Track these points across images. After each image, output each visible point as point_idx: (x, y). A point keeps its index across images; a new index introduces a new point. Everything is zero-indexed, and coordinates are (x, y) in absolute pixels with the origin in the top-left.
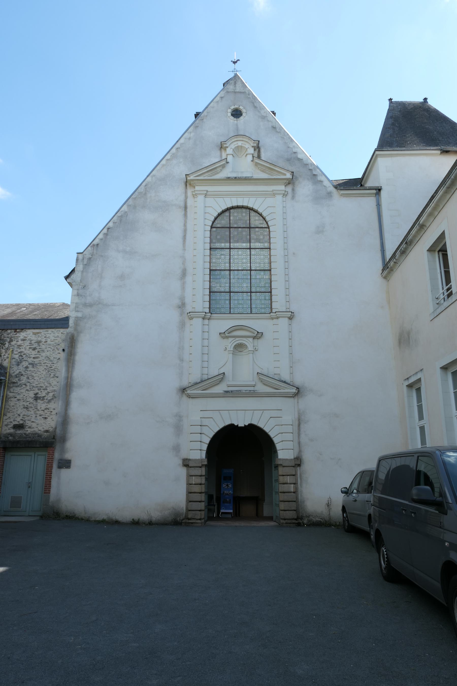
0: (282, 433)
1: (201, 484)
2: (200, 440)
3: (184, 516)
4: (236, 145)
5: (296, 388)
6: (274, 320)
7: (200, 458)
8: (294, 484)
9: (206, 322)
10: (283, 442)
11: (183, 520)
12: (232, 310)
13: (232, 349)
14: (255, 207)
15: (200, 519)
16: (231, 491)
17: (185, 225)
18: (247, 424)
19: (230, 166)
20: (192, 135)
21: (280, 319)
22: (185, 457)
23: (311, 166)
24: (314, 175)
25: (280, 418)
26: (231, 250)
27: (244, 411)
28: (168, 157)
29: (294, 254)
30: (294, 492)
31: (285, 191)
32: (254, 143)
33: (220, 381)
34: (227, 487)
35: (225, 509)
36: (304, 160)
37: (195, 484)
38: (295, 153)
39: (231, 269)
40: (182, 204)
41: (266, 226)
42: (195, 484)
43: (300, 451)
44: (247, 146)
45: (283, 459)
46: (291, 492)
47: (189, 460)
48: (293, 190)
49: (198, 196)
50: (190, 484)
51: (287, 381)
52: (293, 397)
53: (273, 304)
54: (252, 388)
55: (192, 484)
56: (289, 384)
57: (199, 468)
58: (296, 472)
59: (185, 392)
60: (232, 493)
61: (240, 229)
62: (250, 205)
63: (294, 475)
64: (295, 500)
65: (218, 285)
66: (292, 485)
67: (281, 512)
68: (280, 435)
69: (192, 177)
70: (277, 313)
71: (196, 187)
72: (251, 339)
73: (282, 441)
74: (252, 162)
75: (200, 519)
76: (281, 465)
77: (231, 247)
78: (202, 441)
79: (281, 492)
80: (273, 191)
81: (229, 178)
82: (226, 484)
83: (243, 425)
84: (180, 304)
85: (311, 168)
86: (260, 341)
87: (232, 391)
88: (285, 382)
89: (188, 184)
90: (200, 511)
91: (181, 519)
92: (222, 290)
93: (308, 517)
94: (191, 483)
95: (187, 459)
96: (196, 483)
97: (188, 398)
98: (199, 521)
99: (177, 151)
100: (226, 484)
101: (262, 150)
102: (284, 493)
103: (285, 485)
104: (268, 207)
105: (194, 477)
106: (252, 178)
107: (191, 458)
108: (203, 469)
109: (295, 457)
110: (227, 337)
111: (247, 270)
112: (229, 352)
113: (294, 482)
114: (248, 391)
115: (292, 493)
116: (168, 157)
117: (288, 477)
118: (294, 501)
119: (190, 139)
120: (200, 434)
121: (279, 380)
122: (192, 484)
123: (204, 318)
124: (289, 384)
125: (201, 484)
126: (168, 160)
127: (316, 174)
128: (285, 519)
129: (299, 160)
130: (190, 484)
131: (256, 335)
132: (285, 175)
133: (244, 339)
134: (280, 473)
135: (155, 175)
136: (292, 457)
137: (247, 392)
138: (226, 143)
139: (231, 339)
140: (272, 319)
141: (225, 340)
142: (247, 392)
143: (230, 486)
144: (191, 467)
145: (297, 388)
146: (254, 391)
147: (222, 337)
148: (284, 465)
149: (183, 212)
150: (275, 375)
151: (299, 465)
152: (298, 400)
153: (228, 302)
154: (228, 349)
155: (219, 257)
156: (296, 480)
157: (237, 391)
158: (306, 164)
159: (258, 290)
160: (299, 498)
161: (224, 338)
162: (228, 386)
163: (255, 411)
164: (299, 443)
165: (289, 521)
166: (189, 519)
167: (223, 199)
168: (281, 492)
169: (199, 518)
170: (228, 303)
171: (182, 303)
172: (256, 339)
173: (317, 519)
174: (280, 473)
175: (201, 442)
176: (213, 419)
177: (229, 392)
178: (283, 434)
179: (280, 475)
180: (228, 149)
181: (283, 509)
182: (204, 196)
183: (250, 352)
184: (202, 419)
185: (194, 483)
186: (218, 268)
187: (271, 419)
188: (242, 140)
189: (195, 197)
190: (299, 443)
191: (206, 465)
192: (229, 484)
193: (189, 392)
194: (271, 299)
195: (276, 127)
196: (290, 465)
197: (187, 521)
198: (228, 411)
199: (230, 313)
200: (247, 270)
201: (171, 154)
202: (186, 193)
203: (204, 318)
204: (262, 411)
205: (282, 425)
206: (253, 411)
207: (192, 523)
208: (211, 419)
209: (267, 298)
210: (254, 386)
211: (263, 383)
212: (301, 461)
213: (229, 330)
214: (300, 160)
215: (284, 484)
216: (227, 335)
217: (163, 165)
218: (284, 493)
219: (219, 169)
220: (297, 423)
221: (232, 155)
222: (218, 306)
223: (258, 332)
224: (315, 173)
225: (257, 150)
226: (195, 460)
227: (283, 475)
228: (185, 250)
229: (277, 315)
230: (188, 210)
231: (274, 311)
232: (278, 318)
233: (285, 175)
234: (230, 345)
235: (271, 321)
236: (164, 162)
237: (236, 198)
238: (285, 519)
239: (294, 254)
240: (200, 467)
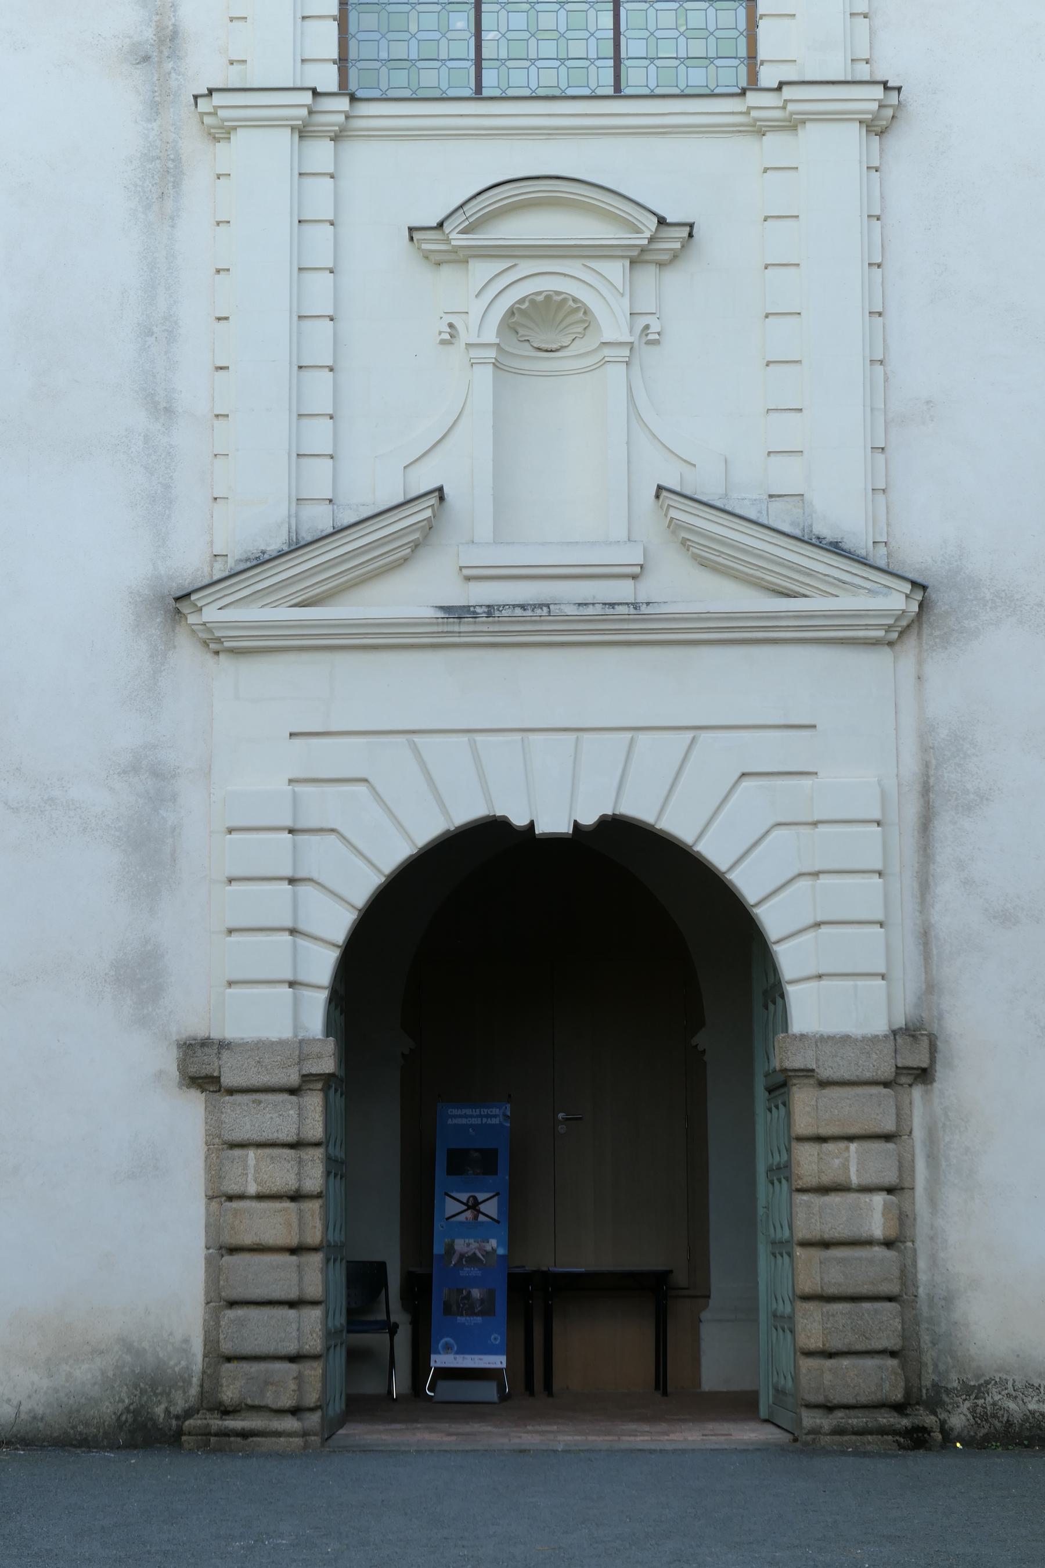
0: (816, 874)
1: (296, 1197)
2: (289, 924)
3: (194, 1391)
5: (907, 588)
6: (769, 138)
7: (287, 1034)
8: (890, 1190)
10: (824, 929)
11: (188, 1413)
12: (489, 77)
13: (490, 335)
15: (295, 1411)
16: (493, 1242)
18: (589, 819)
22: (197, 1027)
25: (806, 782)
27: (572, 737)
30: (888, 1244)
33: (416, 546)
34: (469, 1214)
35: (463, 1350)
37: (260, 1197)
42: (260, 1197)
43: (930, 988)
45: (822, 1040)
46: (869, 1243)
47: (223, 1045)
50: (230, 1198)
51: (847, 545)
52: (890, 644)
54: (622, 591)
55: (241, 1197)
56: (863, 562)
57: (285, 1096)
58: (902, 1115)
59: (192, 619)
60: (501, 1251)
63: (888, 1137)
64: (894, 1289)
66: (878, 1200)
67: (807, 1364)
68: (804, 883)
70: (788, 92)
72: (615, 270)
73: (818, 925)
75: (295, 1411)
76: (808, 1073)
78: (302, 926)
79: (805, 1244)
82: (464, 1197)
83: (564, 827)
84: (149, 34)
86: (674, 279)
87: (491, 610)
88: (836, 548)
90: (293, 1359)
91: (179, 1407)
93: (979, 1391)
94: (233, 1188)
95: (205, 1043)
96: (266, 1191)
97: (210, 659)
98: (290, 1423)
100: (464, 1197)
102: (826, 1244)
103: (834, 1199)
105: (251, 1154)
107: (230, 1033)
108: (314, 1102)
109: (900, 1022)
110: (460, 257)
112: (474, 353)
113: (890, 1177)
114: (598, 610)
115: (876, 1249)
117: (853, 1146)
118: (890, 1299)
120: (292, 881)
121: (797, 532)
122: (241, 1197)
123: (303, 132)
124: (863, 562)
125: (296, 1197)
128: (829, 1408)
130: (230, 1198)
131: (651, 240)
133: (573, 267)
134: (802, 1124)
136: (880, 1026)
137: (590, 611)
139: (481, 270)
140: (759, 129)
141: (447, 273)
142: (590, 611)
143: (491, 1208)
144: (231, 1092)
145: (914, 584)
146: (636, 605)
147: (426, 256)
148: (825, 1073)
150: (776, 505)
151: (924, 1075)
152: (920, 663)
154: (465, 337)
156: (905, 1167)
157: (523, 607)
160: (923, 1277)
161: (436, 261)
162: (468, 579)
163: (643, 737)
164: (925, 936)
165: (857, 1420)
166: (226, 1412)
168: (805, 1244)
169: (287, 1401)
171: (160, 28)
172: (652, 269)
173: (1032, 1406)
174: (802, 1124)
175: (293, 931)
176: (373, 789)
177: (475, 615)
178: (824, 880)
179: (801, 1139)
181: (815, 1343)
183: (607, 351)
184: (300, 788)
185: (252, 1189)
187: (746, 783)
190: (925, 936)
191: (327, 1079)
192: (481, 1197)
193: (211, 614)
196: (868, 1075)
197: (216, 1423)
198: (464, 739)
199: (478, 94)
203: (303, 132)
204: (689, 735)
205: (815, 824)
206: (628, 735)
207: (245, 1434)
208: (361, 789)
210: (634, 577)
211: (695, 557)
212: (933, 1049)
215: (824, 1190)
216: (458, 240)
218: (826, 1244)
220: (912, 811)
222: (399, 51)
223: (662, 221)
226: (261, 1046)
227: (821, 1139)
231: (768, 76)
232: (792, 125)
235: (747, 144)
238: (829, 1408)
240: (293, 1091)
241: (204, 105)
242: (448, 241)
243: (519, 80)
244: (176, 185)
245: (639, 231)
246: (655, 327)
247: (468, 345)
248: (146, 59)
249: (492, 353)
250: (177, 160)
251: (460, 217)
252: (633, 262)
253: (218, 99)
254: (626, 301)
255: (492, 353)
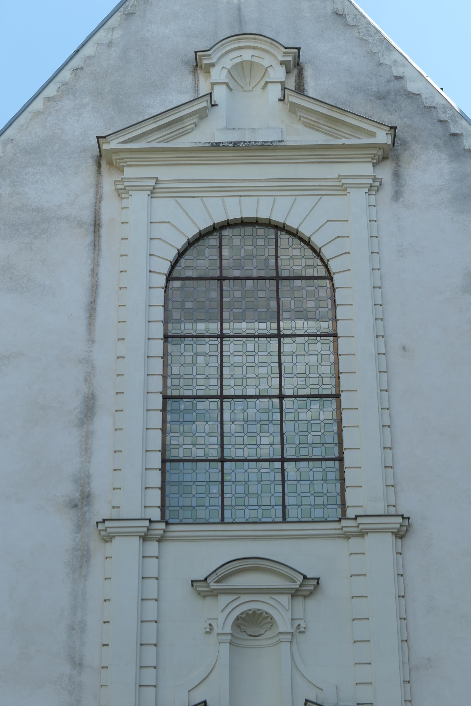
4: (239, 60)
9: (152, 548)
12: (227, 514)
13: (228, 629)
14: (292, 223)
17: (94, 273)
19: (220, 111)
20: (117, 34)
21: (370, 538)
23: (445, 112)
24: (454, 135)
26: (226, 341)
28: (51, 91)
29: (404, 348)
31: (375, 179)
32: (285, 53)
36: (424, 96)
38: (398, 78)
39: (226, 393)
40: (87, 216)
41: (323, 273)
44: (266, 61)
48: (397, 175)
49: (131, 193)
53: (349, 493)
61: (249, 283)
62: (278, 218)
65: (188, 440)
69: (114, 144)
70: (359, 520)
71: (126, 169)
72: (284, 599)
74: (281, 103)
77: (225, 332)
80: (340, 177)
81: (216, 146)
84: (77, 495)
85: (443, 116)
86: (311, 603)
89: (103, 162)
92: (200, 453)
99: (76, 75)
101: (308, 73)
104: (328, 221)
106: (282, 144)
110: (215, 594)
111: (271, 397)
112: (221, 638)
116: (51, 91)
119: (110, 44)
123: (145, 538)
126: (49, 99)
127: (457, 132)
129: (410, 97)
131: (300, 586)
132: (373, 135)
135: (12, 140)
138: (210, 55)
139: (224, 600)
140: (347, 536)
141: (209, 601)
149: (90, 238)
153: (215, 489)
154: (217, 630)
155: (189, 360)
158: (431, 107)
159: (304, 453)
161: (203, 595)
167: (202, 200)
170: (215, 491)
171: (82, 492)
180: (214, 71)
182: (149, 193)
183: (281, 637)
186: (188, 393)
187: (329, 223)
188: (254, 48)
189: (124, 196)
194: (342, 480)
195: (346, 12)
199: (223, 521)
200: (271, 397)
201: (59, 85)
202: (98, 185)
203: (145, 538)
209: (331, 476)
213: (219, 572)
214: (411, 96)
216: (214, 586)
217: (38, 113)
219: (189, 122)
221: (227, 84)
222: (188, 502)
223: (305, 577)
224: (454, 129)
225: (295, 72)
228: (93, 341)
229: (345, 529)
230: (104, 232)
231: (351, 513)
232: (362, 534)
233: (373, 135)
234: (222, 617)
235: (342, 543)
236: (38, 104)
237: (237, 198)
239: (404, 348)
241: (101, 526)
242: (209, 586)
243: (241, 515)
244: (88, 561)
245: (294, 582)
246: (303, 625)
247: (218, 634)
248: (76, 506)
249: (229, 638)
250: (88, 551)
251: (214, 576)
252: (293, 596)
253: (107, 524)
254: (290, 613)
255: (229, 638)
